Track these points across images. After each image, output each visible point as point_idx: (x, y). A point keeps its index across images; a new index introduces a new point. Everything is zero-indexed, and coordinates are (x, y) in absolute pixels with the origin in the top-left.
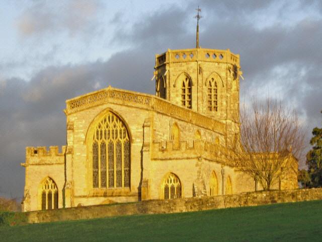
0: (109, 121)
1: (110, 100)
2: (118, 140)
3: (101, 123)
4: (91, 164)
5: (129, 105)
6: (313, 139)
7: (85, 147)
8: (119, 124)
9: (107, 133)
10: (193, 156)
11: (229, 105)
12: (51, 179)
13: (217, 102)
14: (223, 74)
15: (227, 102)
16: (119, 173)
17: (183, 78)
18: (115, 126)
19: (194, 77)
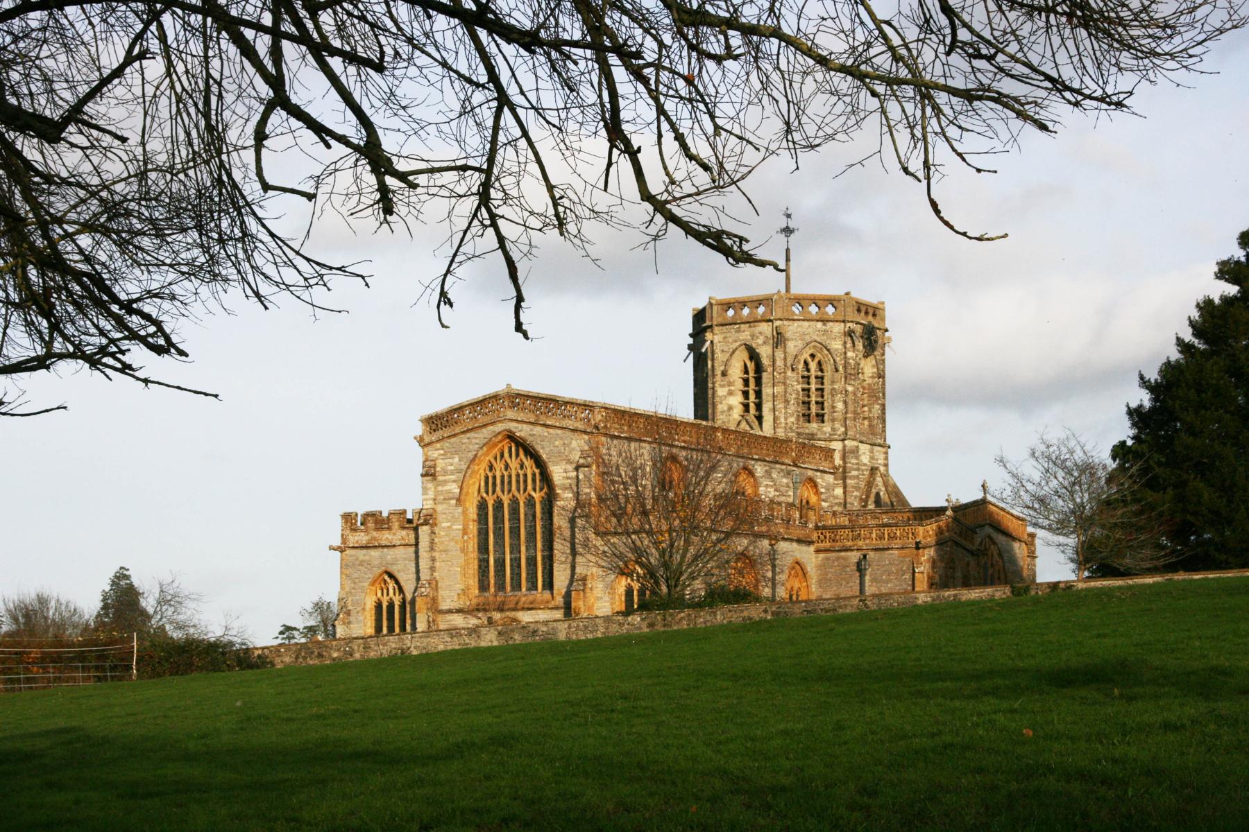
0: (511, 456)
1: (510, 414)
2: (530, 495)
3: (493, 460)
4: (473, 545)
5: (549, 423)
7: (460, 509)
8: (528, 463)
9: (498, 481)
11: (851, 408)
12: (391, 576)
13: (822, 403)
14: (837, 345)
15: (845, 402)
16: (532, 562)
17: (743, 355)
19: (764, 352)
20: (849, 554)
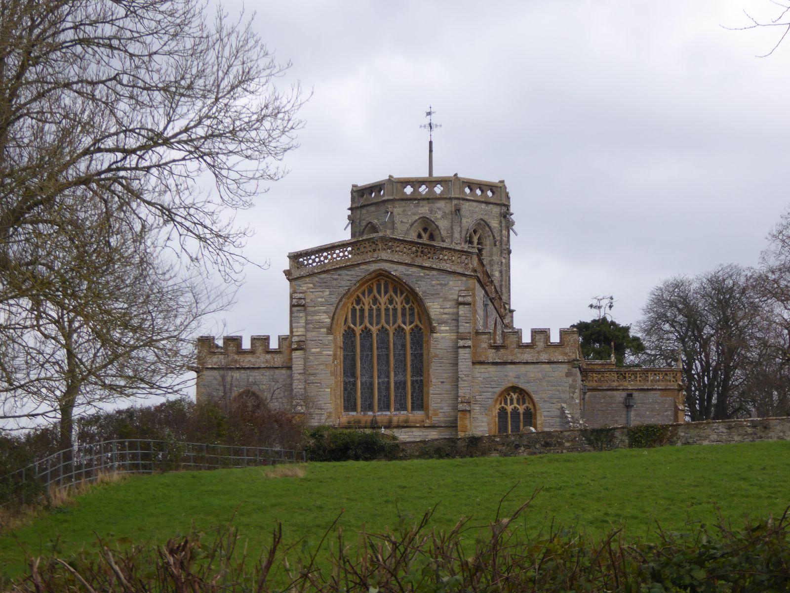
3: (361, 296)
6: (670, 325)
7: (331, 337)
9: (367, 314)
10: (561, 358)
15: (501, 272)
18: (391, 301)
20: (615, 393)
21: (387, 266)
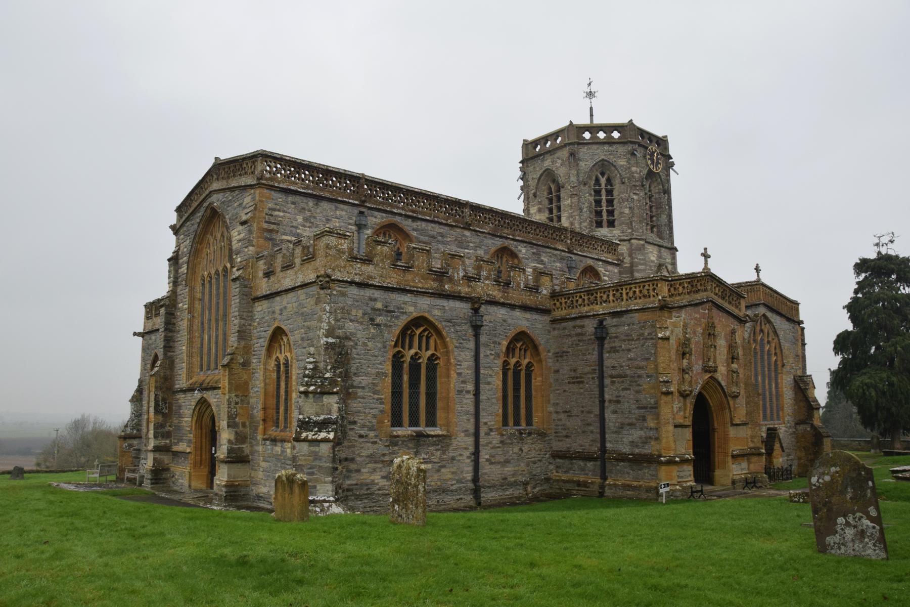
21: (398, 219)
